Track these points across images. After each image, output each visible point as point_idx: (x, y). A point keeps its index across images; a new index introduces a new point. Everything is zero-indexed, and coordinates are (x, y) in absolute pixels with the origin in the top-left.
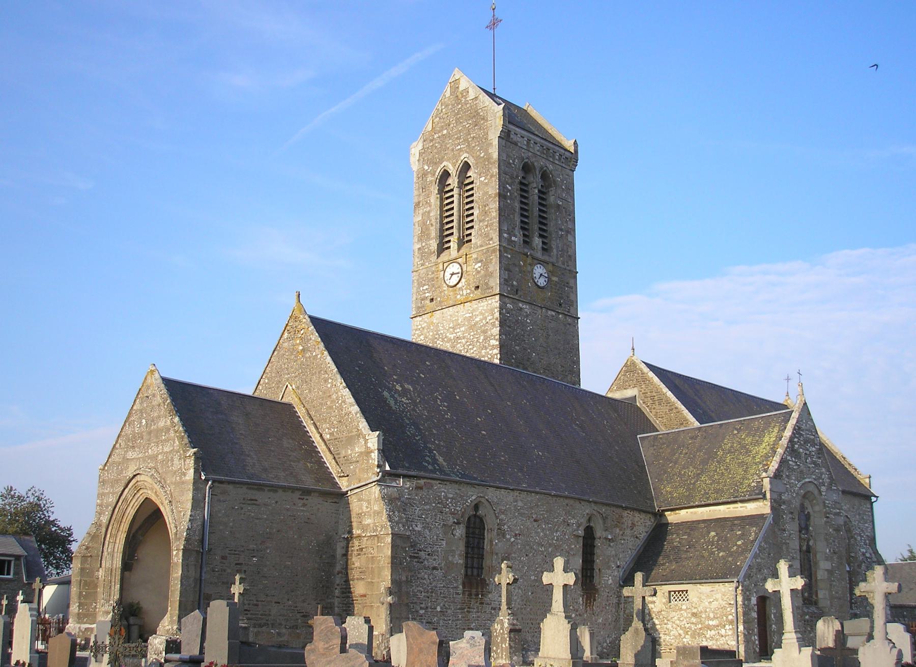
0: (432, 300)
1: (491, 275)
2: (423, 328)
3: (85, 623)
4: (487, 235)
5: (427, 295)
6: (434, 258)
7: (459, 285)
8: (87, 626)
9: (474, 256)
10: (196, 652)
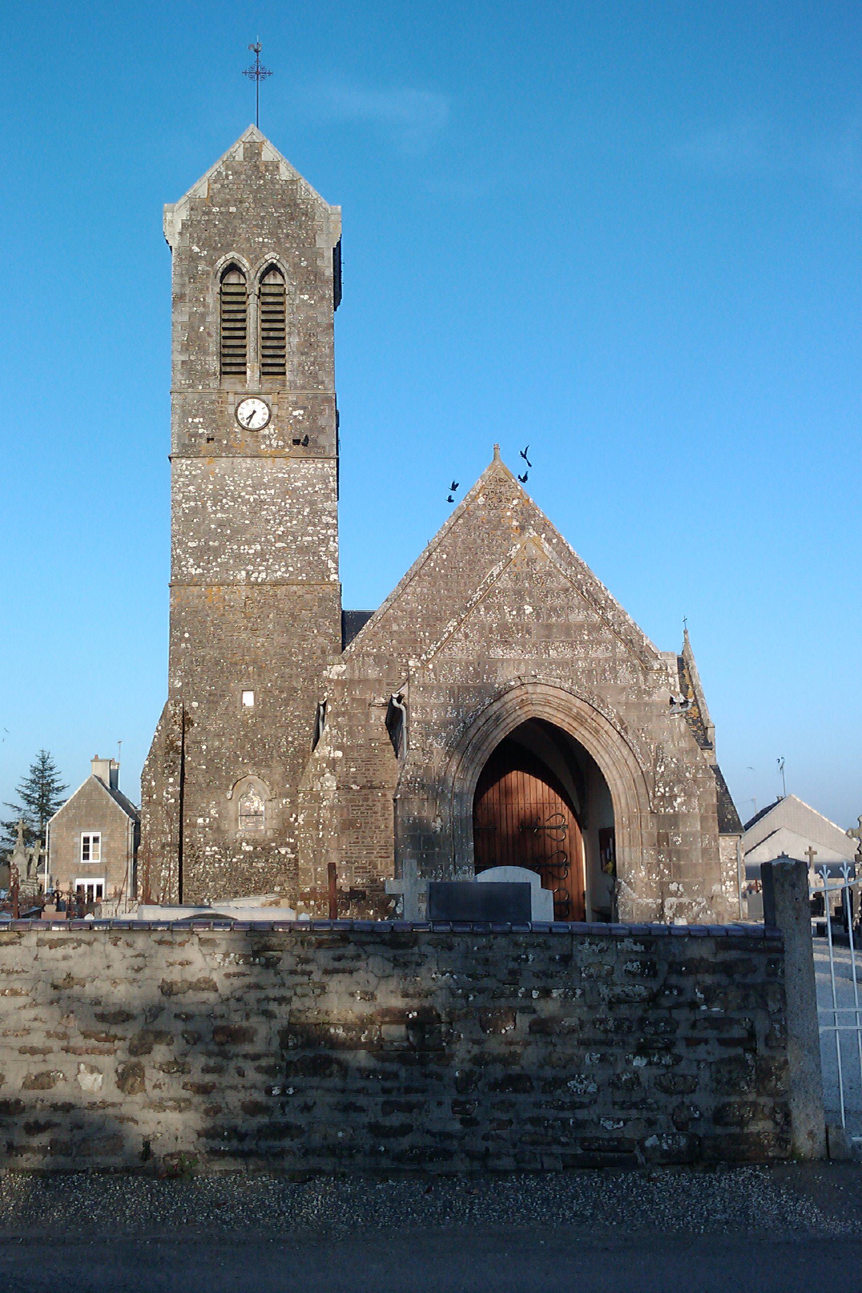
2: (195, 476)
5: (201, 431)
7: (266, 432)
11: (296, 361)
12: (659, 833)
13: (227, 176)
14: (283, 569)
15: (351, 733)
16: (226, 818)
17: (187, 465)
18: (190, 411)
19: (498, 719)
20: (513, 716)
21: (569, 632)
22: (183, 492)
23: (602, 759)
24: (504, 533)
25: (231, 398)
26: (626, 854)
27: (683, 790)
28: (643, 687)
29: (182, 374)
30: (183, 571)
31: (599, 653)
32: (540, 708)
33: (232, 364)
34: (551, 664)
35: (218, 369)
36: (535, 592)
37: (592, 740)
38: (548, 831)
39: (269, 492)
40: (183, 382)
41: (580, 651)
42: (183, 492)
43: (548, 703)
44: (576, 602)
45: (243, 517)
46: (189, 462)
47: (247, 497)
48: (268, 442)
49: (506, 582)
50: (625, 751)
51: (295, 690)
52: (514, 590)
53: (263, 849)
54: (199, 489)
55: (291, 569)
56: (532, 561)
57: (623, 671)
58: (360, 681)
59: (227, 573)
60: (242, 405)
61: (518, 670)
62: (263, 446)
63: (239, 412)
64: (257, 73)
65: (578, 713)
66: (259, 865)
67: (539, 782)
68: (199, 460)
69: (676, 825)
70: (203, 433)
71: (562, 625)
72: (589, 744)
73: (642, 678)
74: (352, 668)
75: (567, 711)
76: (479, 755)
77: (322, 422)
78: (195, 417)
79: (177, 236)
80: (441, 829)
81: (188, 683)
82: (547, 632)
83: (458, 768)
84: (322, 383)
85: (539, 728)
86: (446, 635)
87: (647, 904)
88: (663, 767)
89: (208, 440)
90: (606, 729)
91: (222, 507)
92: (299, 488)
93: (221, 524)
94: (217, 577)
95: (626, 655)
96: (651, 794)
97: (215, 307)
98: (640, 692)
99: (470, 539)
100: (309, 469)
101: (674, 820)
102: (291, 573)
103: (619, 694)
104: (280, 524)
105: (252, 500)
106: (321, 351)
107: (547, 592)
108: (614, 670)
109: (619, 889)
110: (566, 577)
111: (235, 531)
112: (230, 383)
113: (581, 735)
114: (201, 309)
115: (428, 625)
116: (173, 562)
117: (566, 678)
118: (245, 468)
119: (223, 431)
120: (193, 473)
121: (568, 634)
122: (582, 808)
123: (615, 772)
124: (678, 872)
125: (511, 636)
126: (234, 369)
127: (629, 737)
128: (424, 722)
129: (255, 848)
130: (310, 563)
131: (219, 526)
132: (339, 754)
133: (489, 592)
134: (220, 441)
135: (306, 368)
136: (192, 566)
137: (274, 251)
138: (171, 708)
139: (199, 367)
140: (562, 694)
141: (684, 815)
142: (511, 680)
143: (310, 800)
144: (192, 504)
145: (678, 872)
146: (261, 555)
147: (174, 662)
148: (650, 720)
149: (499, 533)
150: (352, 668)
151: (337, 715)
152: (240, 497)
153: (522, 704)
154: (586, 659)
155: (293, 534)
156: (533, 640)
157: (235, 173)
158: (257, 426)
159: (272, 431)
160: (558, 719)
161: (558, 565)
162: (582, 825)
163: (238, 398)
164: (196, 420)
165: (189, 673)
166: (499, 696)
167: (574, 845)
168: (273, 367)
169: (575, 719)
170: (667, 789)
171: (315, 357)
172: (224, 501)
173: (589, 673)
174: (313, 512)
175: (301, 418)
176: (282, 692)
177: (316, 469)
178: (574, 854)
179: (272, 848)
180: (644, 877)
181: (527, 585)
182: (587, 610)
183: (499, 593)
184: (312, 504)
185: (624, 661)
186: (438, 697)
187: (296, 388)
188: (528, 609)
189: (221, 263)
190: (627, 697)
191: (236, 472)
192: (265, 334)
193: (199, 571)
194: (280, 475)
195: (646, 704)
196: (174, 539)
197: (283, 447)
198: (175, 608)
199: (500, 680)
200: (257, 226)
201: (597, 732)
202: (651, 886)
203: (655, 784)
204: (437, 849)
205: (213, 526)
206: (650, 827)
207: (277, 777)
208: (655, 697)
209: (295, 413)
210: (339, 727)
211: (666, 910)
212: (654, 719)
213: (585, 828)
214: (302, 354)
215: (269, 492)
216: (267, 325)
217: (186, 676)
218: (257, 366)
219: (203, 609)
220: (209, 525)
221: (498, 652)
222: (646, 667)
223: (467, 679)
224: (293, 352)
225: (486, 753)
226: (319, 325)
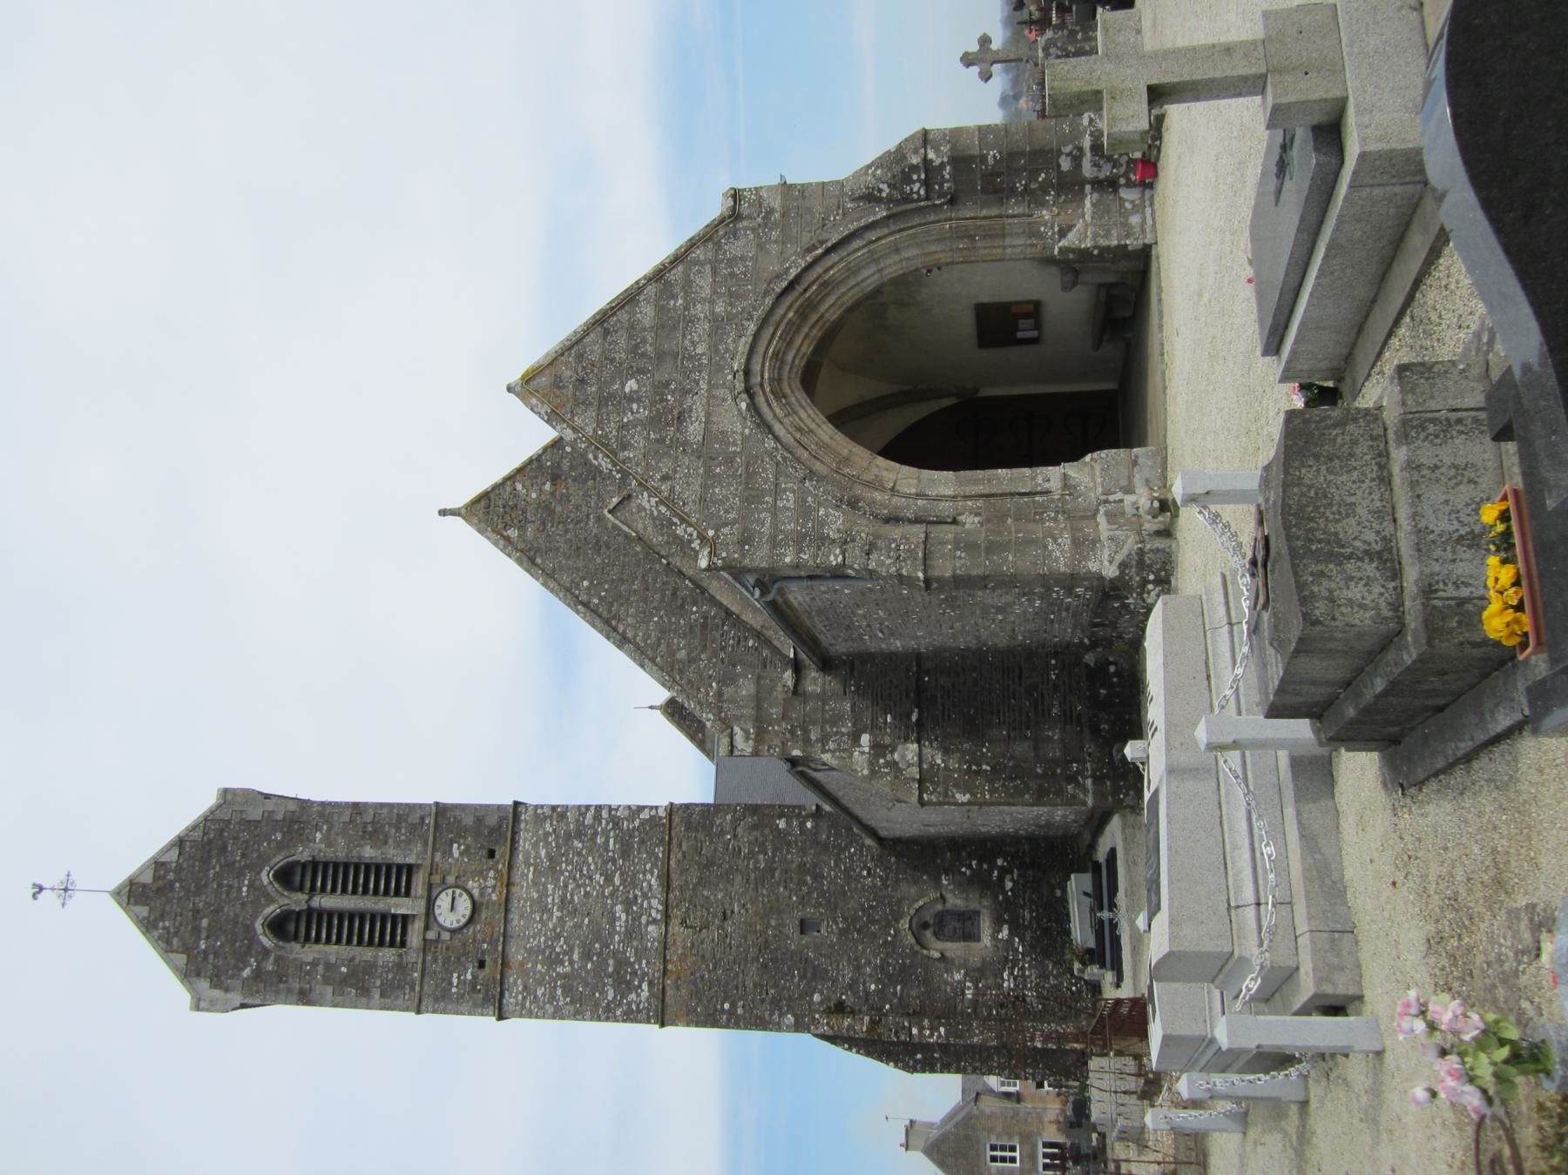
0: (482, 964)
5: (469, 977)
7: (476, 893)
13: (164, 928)
14: (649, 876)
15: (836, 720)
16: (966, 961)
18: (444, 990)
19: (799, 429)
24: (560, 502)
29: (397, 998)
31: (704, 284)
33: (391, 930)
34: (717, 351)
35: (393, 951)
41: (700, 310)
44: (626, 317)
45: (581, 926)
50: (857, 243)
51: (802, 865)
53: (1006, 910)
54: (540, 983)
55: (648, 866)
58: (759, 707)
61: (724, 400)
62: (494, 897)
64: (66, 890)
66: (1027, 916)
69: (970, 159)
73: (745, 223)
74: (737, 718)
75: (794, 328)
78: (451, 984)
79: (229, 996)
82: (668, 358)
86: (663, 509)
87: (1093, 205)
91: (565, 953)
92: (548, 854)
93: (587, 955)
99: (564, 547)
102: (654, 865)
103: (768, 252)
104: (591, 878)
108: (731, 262)
109: (1073, 251)
111: (598, 936)
114: (320, 968)
115: (682, 606)
125: (671, 411)
129: (1006, 922)
130: (642, 841)
131: (590, 958)
132: (865, 739)
133: (601, 444)
134: (484, 953)
136: (638, 995)
137: (259, 873)
138: (821, 1030)
144: (559, 992)
146: (628, 904)
148: (809, 210)
149: (559, 509)
150: (737, 718)
151: (807, 741)
154: (712, 302)
155: (605, 862)
157: (162, 917)
164: (455, 981)
165: (776, 1004)
168: (397, 878)
173: (733, 297)
174: (579, 834)
176: (805, 883)
177: (527, 831)
179: (1006, 899)
184: (568, 836)
185: (720, 248)
188: (631, 385)
189: (267, 941)
193: (645, 986)
197: (497, 871)
200: (228, 893)
201: (825, 284)
203: (907, 199)
207: (913, 890)
209: (456, 853)
210: (824, 740)
211: (1102, 176)
218: (393, 901)
219: (695, 983)
220: (587, 972)
223: (734, 476)
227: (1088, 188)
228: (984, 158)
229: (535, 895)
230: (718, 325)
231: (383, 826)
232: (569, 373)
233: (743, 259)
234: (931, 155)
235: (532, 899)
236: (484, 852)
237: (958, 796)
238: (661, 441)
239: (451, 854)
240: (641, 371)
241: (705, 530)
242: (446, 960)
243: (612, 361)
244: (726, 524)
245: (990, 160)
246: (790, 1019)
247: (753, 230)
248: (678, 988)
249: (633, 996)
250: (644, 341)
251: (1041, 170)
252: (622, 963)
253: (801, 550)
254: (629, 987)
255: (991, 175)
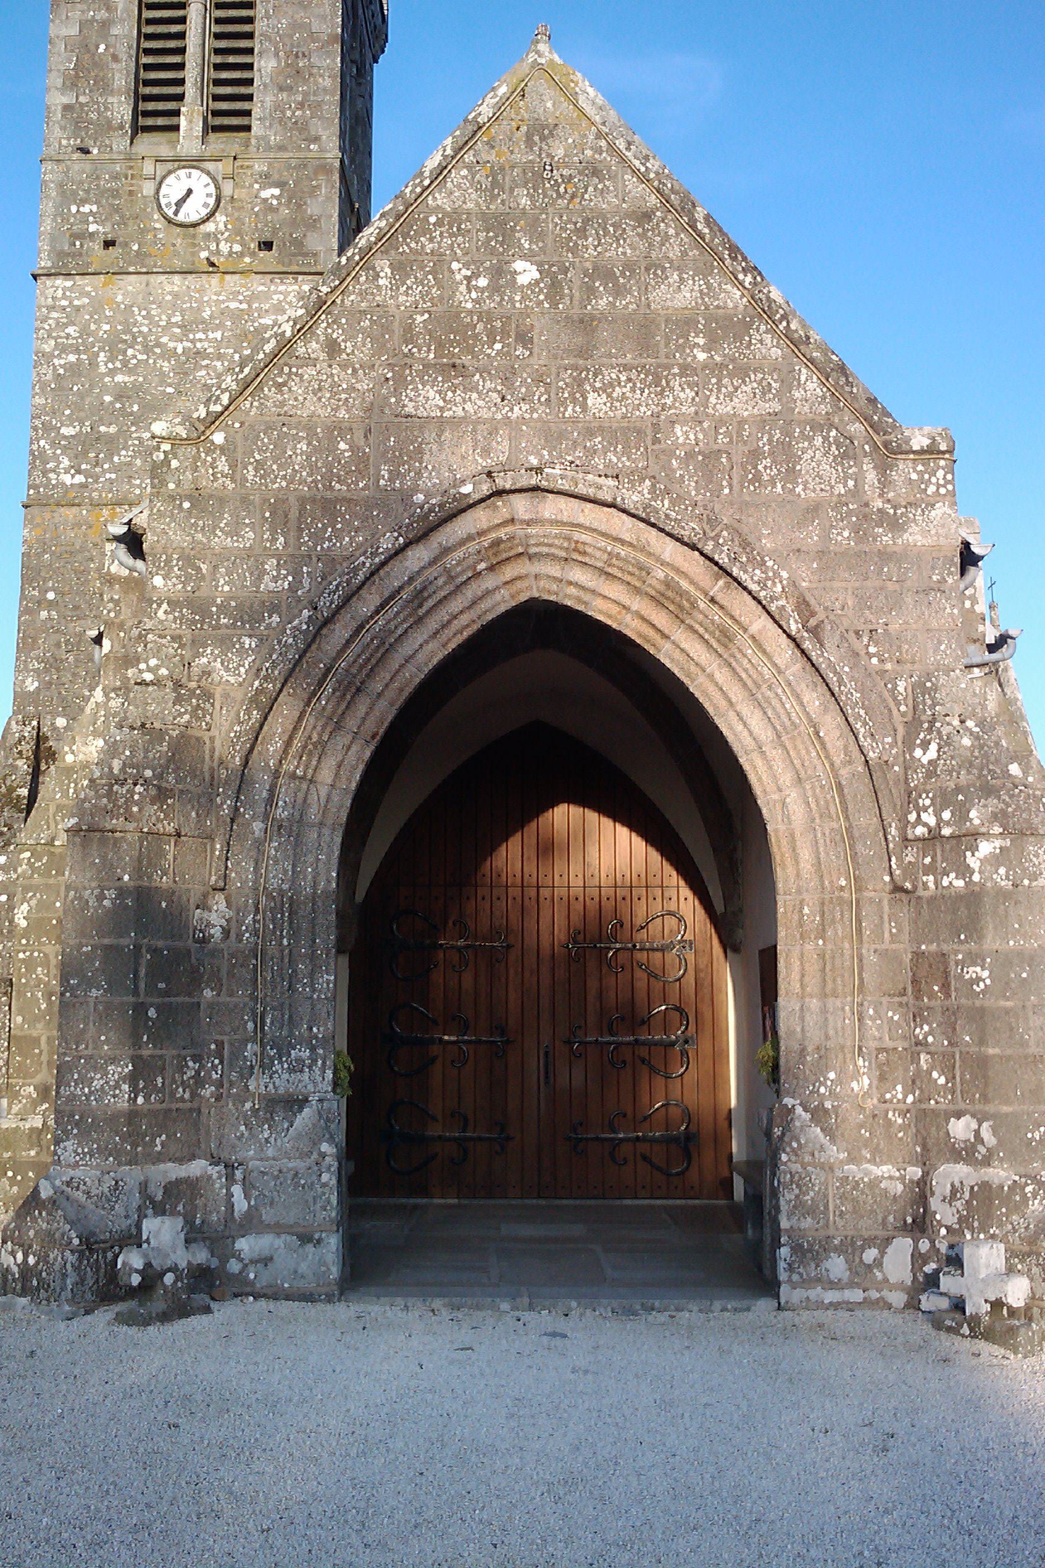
0: (108, 244)
1: (313, 224)
2: (78, 309)
3: (159, 1158)
4: (301, 127)
5: (92, 228)
6: (120, 143)
7: (210, 227)
8: (174, 1171)
9: (259, 167)
10: (943, 1289)
11: (269, 99)
12: (918, 955)
17: (64, 289)
18: (75, 193)
19: (419, 597)
20: (470, 592)
21: (650, 342)
22: (56, 339)
23: (746, 729)
25: (148, 168)
26: (811, 1020)
27: (999, 817)
28: (879, 504)
29: (63, 128)
30: (49, 480)
31: (741, 402)
32: (554, 570)
33: (153, 111)
34: (590, 433)
35: (128, 117)
36: (552, 224)
37: (714, 666)
38: (642, 957)
39: (211, 335)
40: (64, 142)
42: (56, 339)
43: (575, 555)
44: (674, 252)
45: (162, 382)
46: (69, 284)
47: (171, 345)
48: (213, 247)
49: (460, 193)
50: (814, 699)
52: (484, 217)
54: (84, 331)
56: (541, 132)
57: (816, 461)
59: (129, 482)
60: (168, 181)
61: (486, 452)
63: (161, 194)
65: (668, 583)
67: (623, 832)
68: (87, 279)
69: (973, 927)
70: (98, 232)
71: (627, 319)
72: (702, 679)
73: (871, 476)
75: (634, 576)
76: (361, 708)
77: (313, 208)
78: (84, 202)
80: (226, 932)
81: (51, 684)
82: (579, 340)
83: (288, 744)
84: (316, 139)
85: (549, 629)
87: (875, 1183)
88: (933, 747)
89: (108, 244)
90: (754, 629)
91: (125, 363)
93: (122, 394)
94: (111, 491)
95: (823, 409)
96: (893, 831)
97: (126, 10)
98: (866, 520)
100: (286, 294)
101: (968, 911)
103: (800, 525)
105: (180, 351)
106: (316, 83)
107: (587, 221)
109: (787, 1128)
110: (644, 179)
112: (150, 145)
113: (683, 654)
114: (103, 14)
116: (32, 464)
117: (637, 476)
118: (170, 293)
119: (132, 227)
120: (76, 302)
121: (645, 345)
122: (727, 899)
123: (779, 766)
124: (976, 1079)
126: (160, 121)
127: (828, 656)
128: (190, 603)
135: (289, 113)
139: (93, 116)
140: (623, 526)
141: (1003, 895)
142: (463, 482)
143: (48, 867)
144: (72, 358)
145: (976, 1079)
147: (26, 643)
148: (895, 603)
152: (158, 345)
153: (499, 554)
154: (697, 419)
156: (536, 363)
158: (194, 218)
159: (221, 226)
160: (611, 605)
161: (621, 144)
162: (730, 945)
163: (161, 169)
164: (86, 209)
165: (53, 664)
166: (426, 528)
167: (706, 990)
168: (229, 116)
169: (658, 601)
170: (946, 815)
171: (305, 94)
172: (130, 352)
173: (707, 461)
175: (275, 202)
178: (708, 1015)
180: (867, 1094)
181: (524, 201)
182: (705, 272)
183: (439, 223)
185: (817, 427)
186: (234, 532)
187: (269, 148)
188: (526, 272)
190: (826, 537)
191: (152, 302)
192: (219, 59)
193: (80, 479)
194: (233, 305)
195: (885, 556)
196: (37, 422)
197: (242, 255)
198: (30, 548)
199: (429, 481)
202: (889, 1123)
203: (910, 798)
204: (208, 993)
205: (108, 399)
206: (890, 934)
208: (914, 536)
209: (266, 194)
211: (934, 1203)
212: (909, 600)
213: (736, 949)
214: (281, 89)
215: (211, 335)
216: (223, 44)
217: (46, 670)
219: (82, 549)
220: (100, 396)
221: (427, 398)
222: (886, 445)
223: (329, 477)
224: (265, 85)
225: (383, 704)
226: (313, 37)
227: (915, 1172)
228: (974, 959)
229: (206, 315)
230: (647, 435)
231: (305, 81)
232: (560, 152)
233: (791, 475)
234: (985, 848)
235: (199, 310)
236: (267, 236)
237: (25, 907)
238: (409, 335)
239: (263, 188)
240: (555, 290)
241: (226, 428)
242: (115, 194)
243: (582, 233)
244: (233, 466)
245: (973, 971)
246: (31, 685)
247: (856, 493)
248: (77, 525)
249: (66, 462)
250: (619, 291)
251: (951, 1078)
252: (112, 444)
253: (173, 604)
254: (78, 458)
255: (946, 974)
